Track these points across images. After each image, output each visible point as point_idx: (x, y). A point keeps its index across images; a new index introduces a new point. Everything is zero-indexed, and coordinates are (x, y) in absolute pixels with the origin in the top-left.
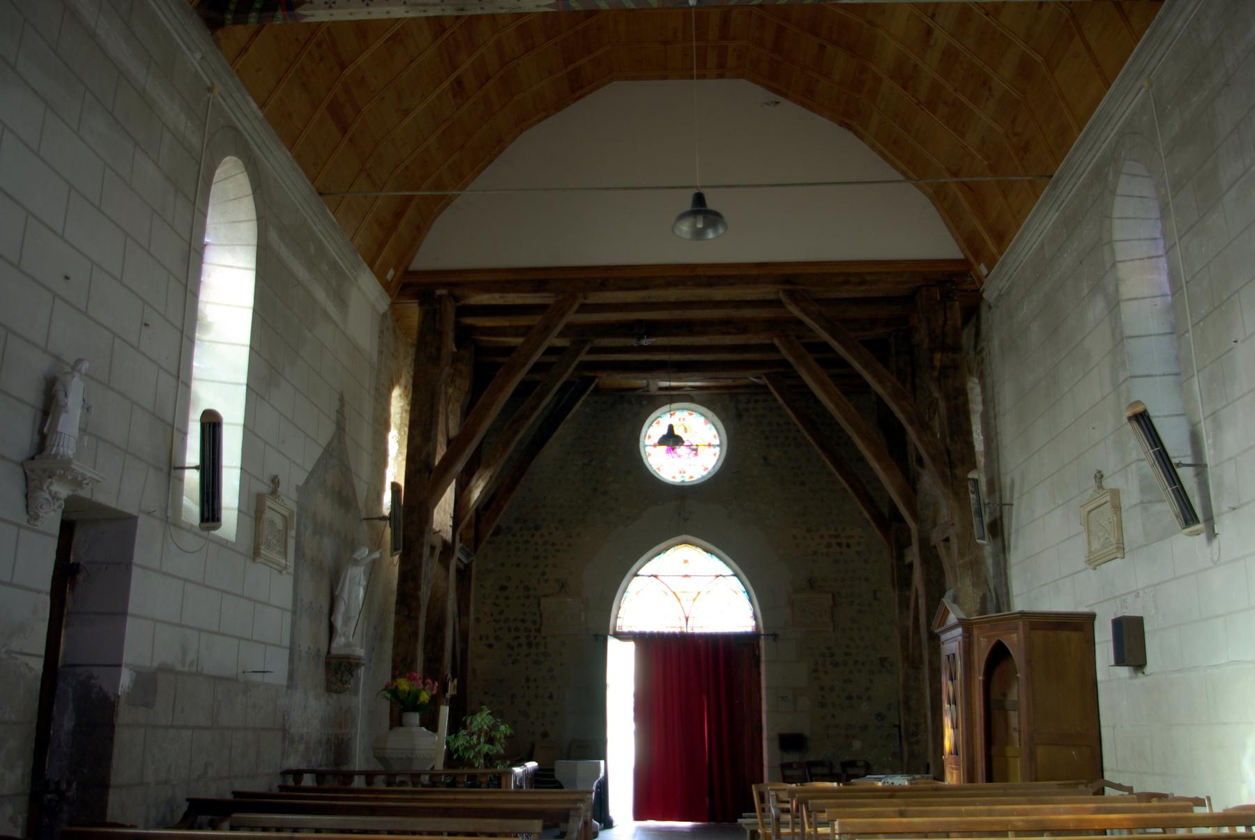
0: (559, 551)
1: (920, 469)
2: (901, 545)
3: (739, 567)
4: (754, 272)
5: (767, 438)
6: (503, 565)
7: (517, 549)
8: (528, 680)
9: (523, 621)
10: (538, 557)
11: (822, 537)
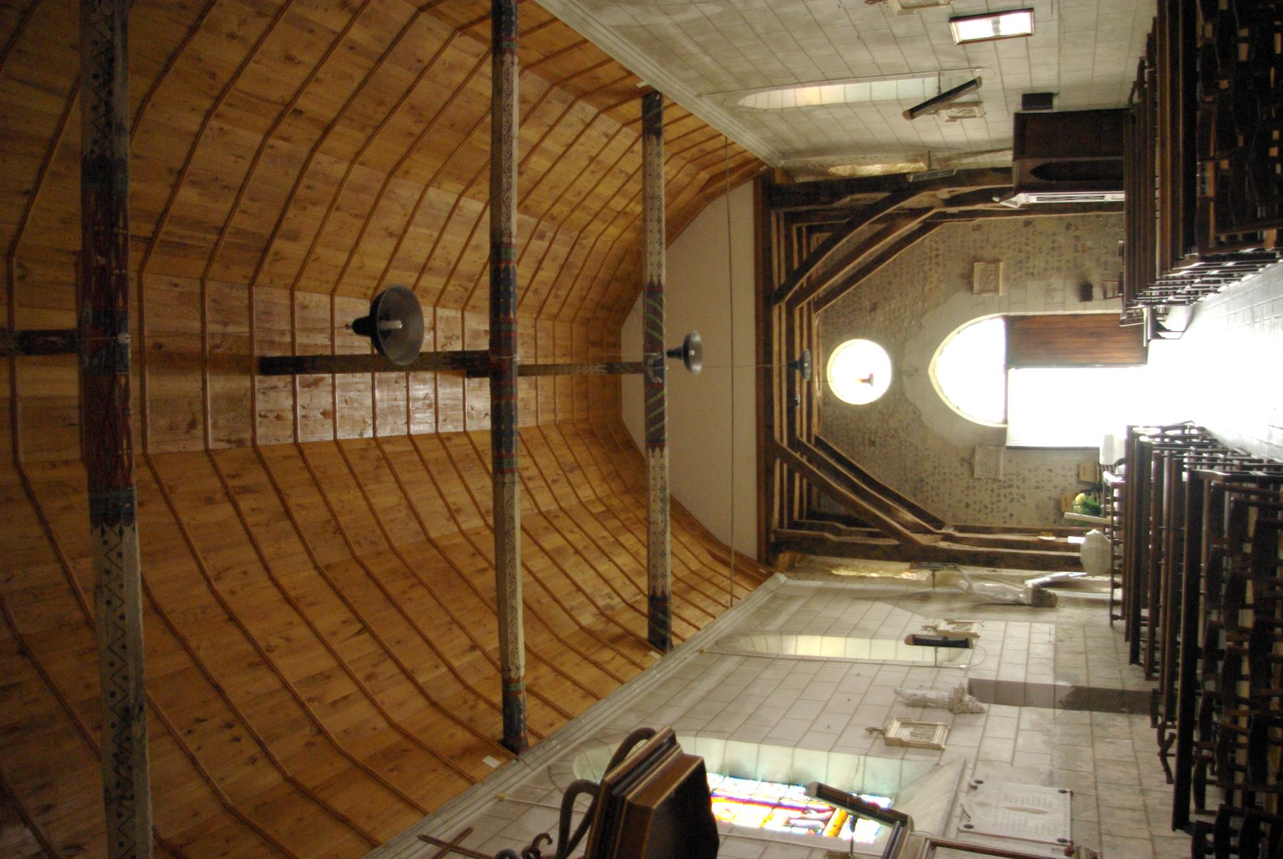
2: (944, 216)
6: (949, 506)
7: (938, 495)
8: (1037, 488)
9: (992, 491)
11: (931, 269)
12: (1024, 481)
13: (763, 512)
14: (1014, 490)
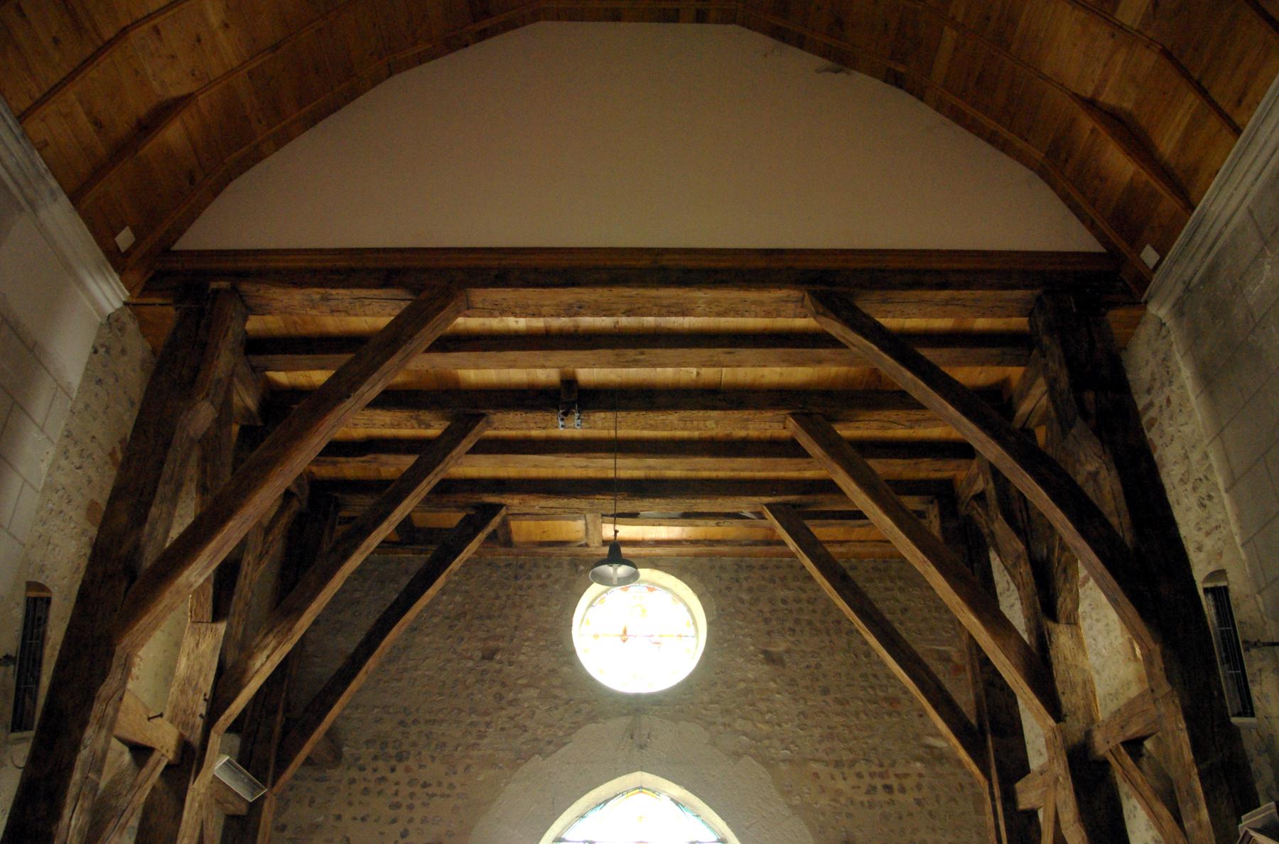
0: (433, 795)
1: (1051, 624)
3: (728, 824)
4: (761, 263)
5: (767, 621)
7: (366, 791)
10: (397, 806)
11: (859, 775)
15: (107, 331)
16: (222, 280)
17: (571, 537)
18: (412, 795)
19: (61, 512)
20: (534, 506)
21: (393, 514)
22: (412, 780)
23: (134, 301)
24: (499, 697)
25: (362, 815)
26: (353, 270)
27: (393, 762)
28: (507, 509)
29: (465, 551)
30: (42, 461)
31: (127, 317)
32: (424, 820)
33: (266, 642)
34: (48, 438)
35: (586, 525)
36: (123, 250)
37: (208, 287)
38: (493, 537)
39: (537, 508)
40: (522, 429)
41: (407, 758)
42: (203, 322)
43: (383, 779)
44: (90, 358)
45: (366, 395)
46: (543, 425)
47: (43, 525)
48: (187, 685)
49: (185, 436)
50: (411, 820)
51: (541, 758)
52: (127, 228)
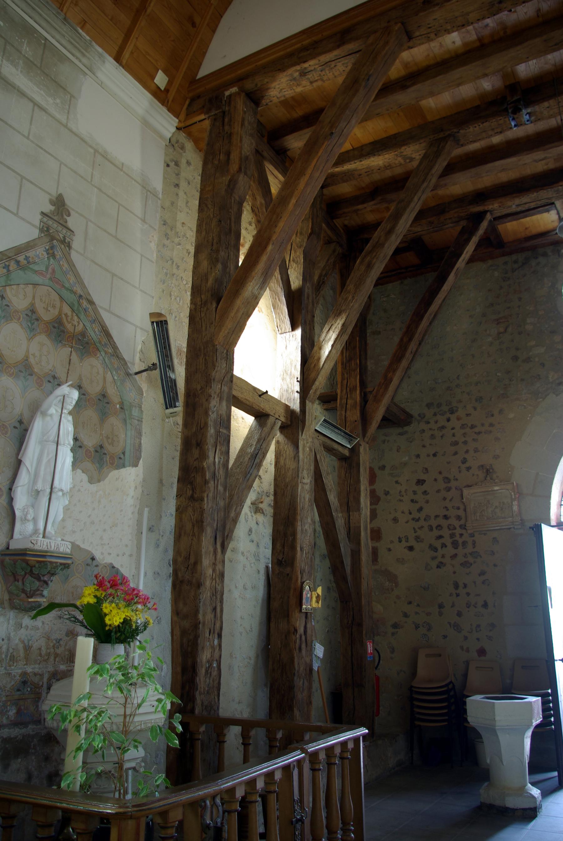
0: (479, 433)
7: (433, 437)
10: (456, 443)
12: (465, 564)
13: (20, 552)
14: (450, 550)
15: (171, 150)
16: (232, 88)
17: (550, 226)
18: (464, 434)
19: (173, 275)
20: (510, 207)
21: (397, 228)
22: (463, 425)
23: (182, 125)
24: (515, 358)
25: (433, 452)
26: (316, 42)
27: (448, 415)
28: (491, 214)
29: (465, 252)
30: (151, 242)
31: (182, 137)
32: (476, 450)
33: (328, 337)
34: (151, 226)
35: (558, 213)
36: (163, 89)
37: (224, 94)
38: (485, 242)
39: (514, 206)
40: (483, 139)
41: (457, 411)
42: (226, 120)
43: (443, 427)
44: (165, 173)
45: (345, 131)
46: (499, 130)
47: (163, 284)
48: (285, 374)
49: (233, 201)
50: (467, 452)
51: (554, 396)
52: (160, 71)
